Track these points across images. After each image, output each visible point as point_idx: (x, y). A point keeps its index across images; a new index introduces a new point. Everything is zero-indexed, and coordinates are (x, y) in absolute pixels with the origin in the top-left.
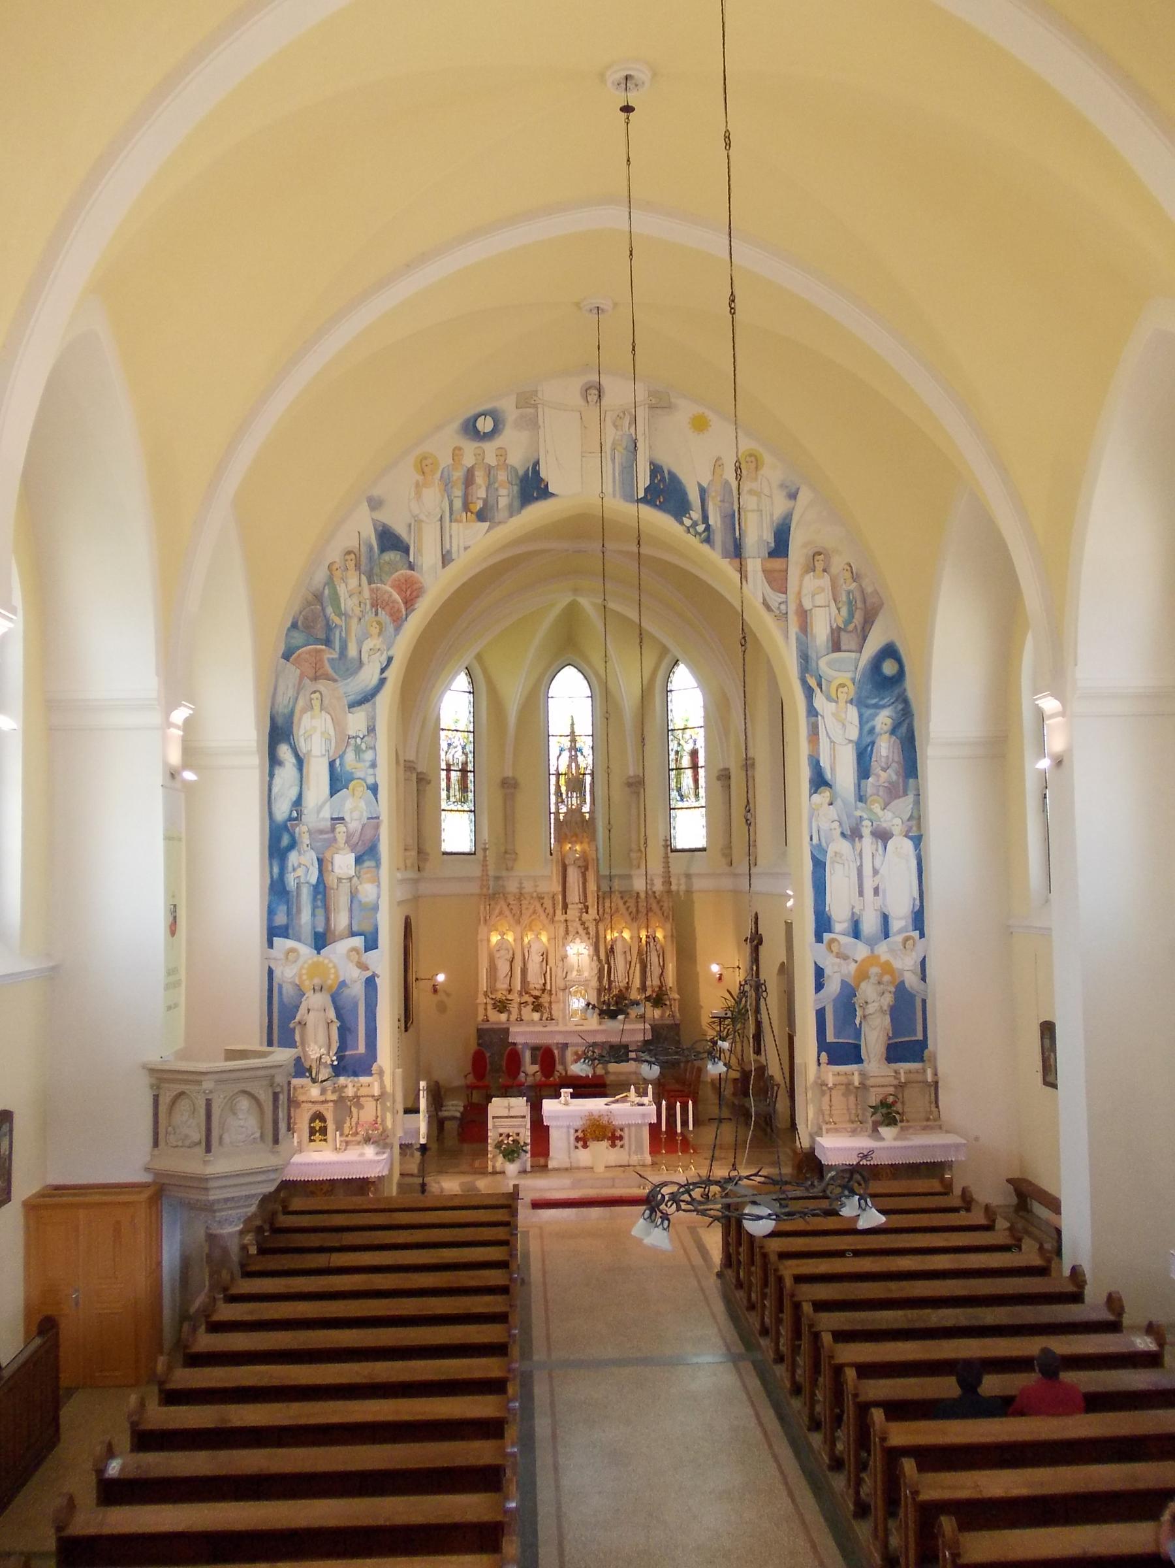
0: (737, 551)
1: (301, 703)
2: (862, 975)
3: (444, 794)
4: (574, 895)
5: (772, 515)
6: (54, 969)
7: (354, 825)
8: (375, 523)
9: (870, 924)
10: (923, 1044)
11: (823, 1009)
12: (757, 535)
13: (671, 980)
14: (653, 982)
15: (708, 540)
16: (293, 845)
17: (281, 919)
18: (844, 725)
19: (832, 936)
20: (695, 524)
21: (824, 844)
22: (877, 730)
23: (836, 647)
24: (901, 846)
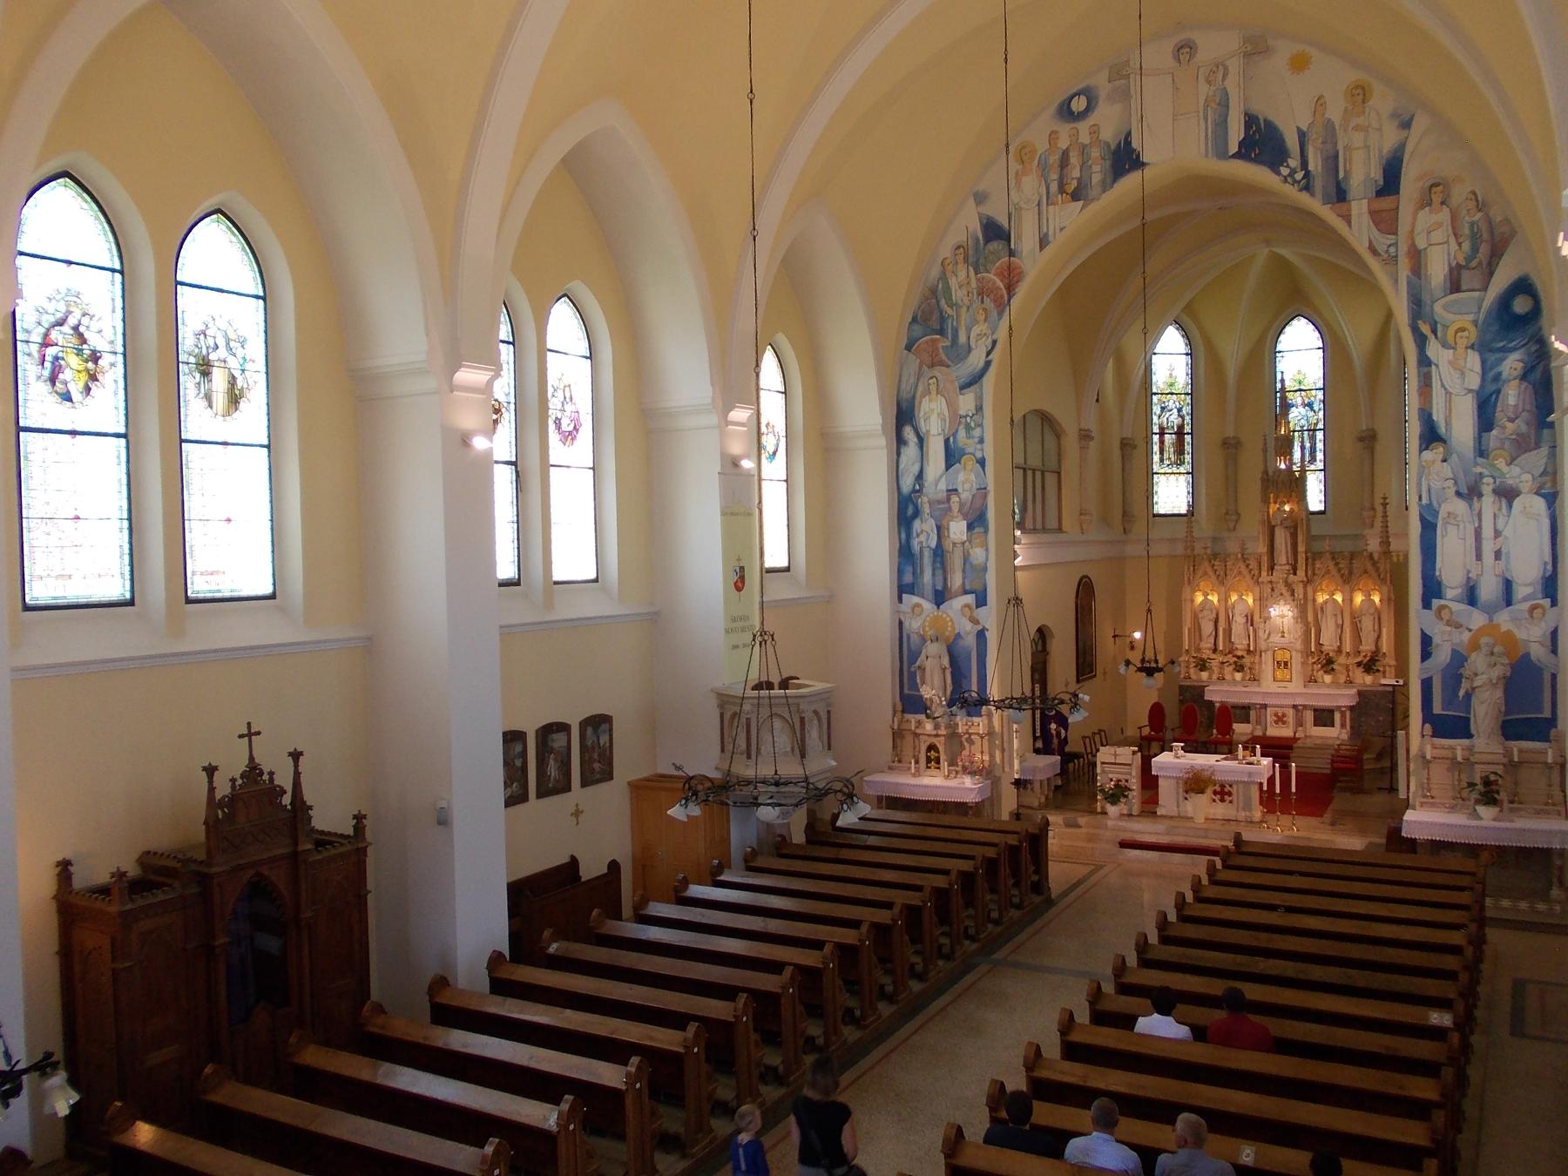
0: (1340, 195)
1: (920, 388)
2: (1475, 646)
3: (1156, 458)
4: (1282, 557)
5: (1380, 151)
6: (656, 613)
7: (966, 496)
8: (980, 216)
9: (1489, 589)
10: (1552, 721)
11: (1431, 678)
12: (1362, 173)
13: (1386, 645)
14: (1367, 646)
15: (1307, 188)
16: (917, 513)
17: (908, 578)
18: (1463, 373)
19: (1442, 602)
20: (1293, 172)
21: (1435, 504)
22: (1504, 376)
23: (1455, 286)
24: (1532, 505)
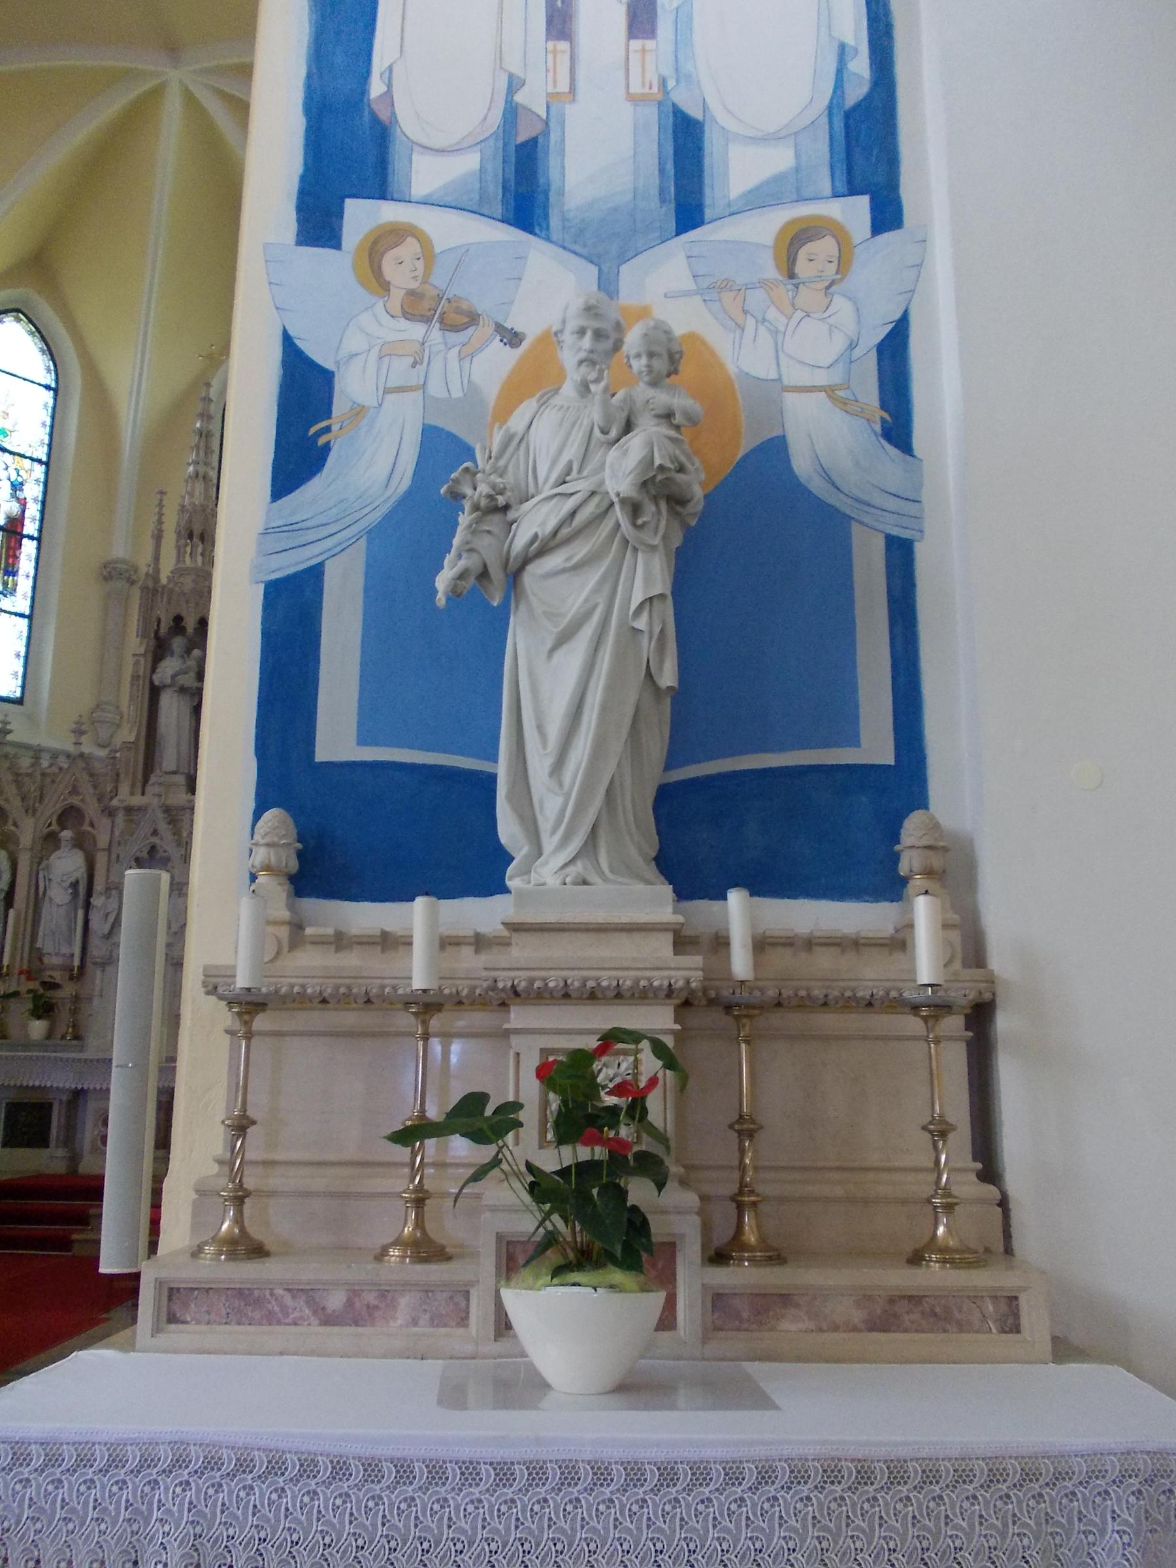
9: (604, 157)
10: (904, 782)
11: (315, 574)
19: (389, 212)
